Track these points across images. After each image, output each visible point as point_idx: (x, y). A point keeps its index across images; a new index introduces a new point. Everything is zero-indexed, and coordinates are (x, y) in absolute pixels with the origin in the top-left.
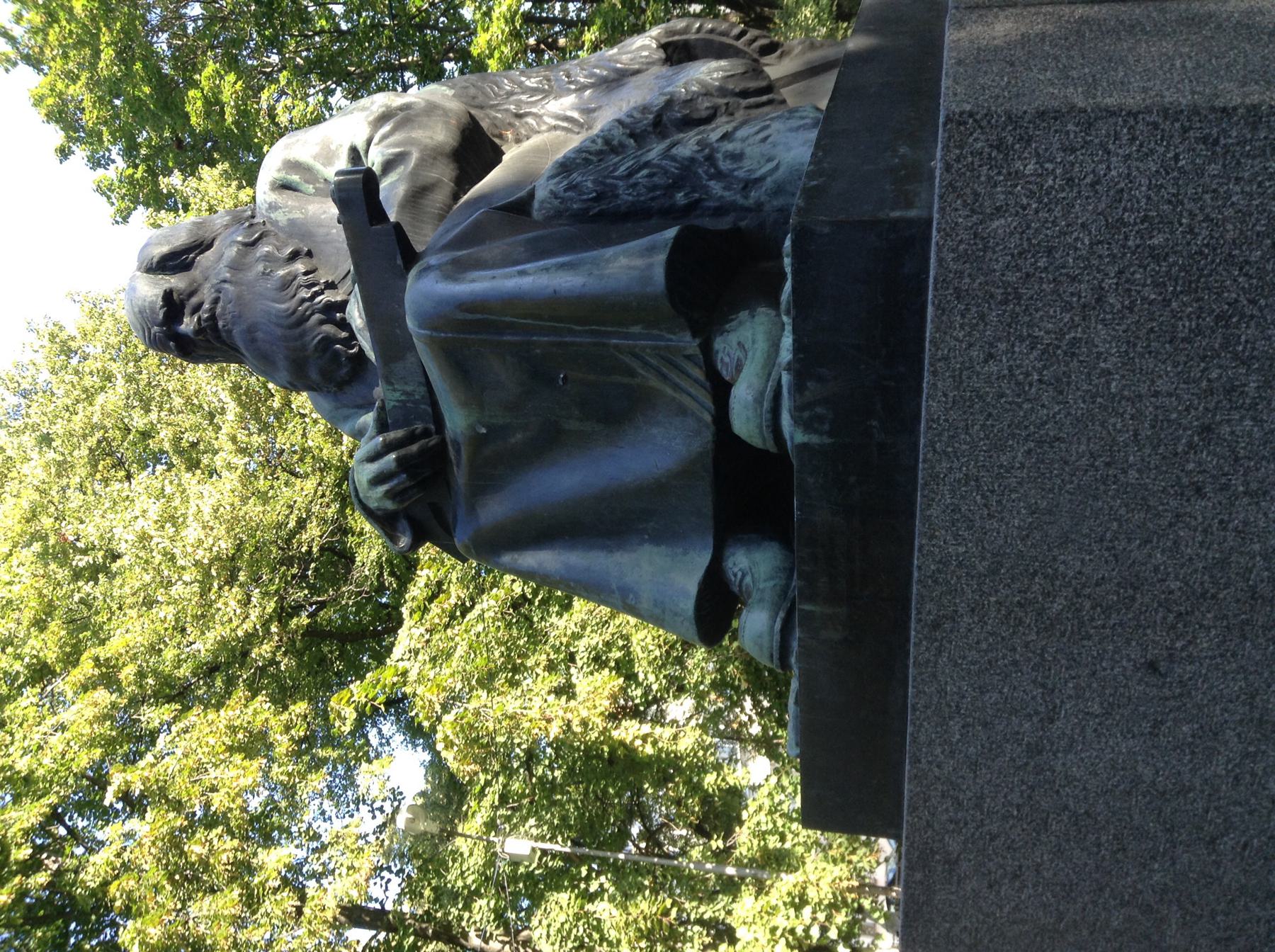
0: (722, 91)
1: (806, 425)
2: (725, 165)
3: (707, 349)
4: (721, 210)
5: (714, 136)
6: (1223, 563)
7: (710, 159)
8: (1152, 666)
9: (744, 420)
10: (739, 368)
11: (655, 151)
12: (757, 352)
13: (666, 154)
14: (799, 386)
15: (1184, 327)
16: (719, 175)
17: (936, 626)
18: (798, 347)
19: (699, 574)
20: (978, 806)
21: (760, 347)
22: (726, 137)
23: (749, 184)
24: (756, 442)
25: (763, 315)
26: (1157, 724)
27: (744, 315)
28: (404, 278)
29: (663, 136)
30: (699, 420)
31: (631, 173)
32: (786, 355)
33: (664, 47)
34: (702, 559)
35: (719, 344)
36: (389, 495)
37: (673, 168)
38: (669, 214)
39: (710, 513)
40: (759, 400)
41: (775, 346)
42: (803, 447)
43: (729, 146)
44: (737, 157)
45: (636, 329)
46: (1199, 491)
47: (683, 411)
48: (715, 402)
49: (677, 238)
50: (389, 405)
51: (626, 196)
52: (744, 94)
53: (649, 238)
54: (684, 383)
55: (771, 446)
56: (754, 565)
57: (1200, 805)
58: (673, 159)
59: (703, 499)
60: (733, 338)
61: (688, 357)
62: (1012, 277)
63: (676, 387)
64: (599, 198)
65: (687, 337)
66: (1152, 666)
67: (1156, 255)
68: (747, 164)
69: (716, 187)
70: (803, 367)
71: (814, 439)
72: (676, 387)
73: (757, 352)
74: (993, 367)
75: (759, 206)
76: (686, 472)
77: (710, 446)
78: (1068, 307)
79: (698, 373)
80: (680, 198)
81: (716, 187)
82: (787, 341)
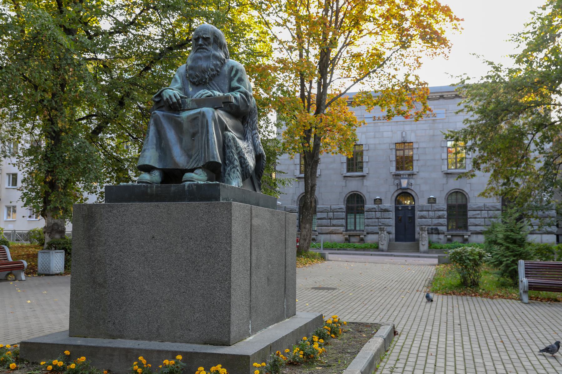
0: (246, 169)
1: (189, 186)
2: (232, 170)
3: (200, 168)
4: (225, 170)
5: (238, 168)
6: (171, 244)
7: (234, 167)
9: (188, 175)
10: (196, 174)
11: (236, 157)
12: (199, 177)
13: (235, 159)
14: (195, 185)
15: (205, 233)
17: (158, 206)
18: (201, 184)
19: (153, 165)
21: (200, 178)
22: (238, 170)
23: (229, 174)
24: (184, 177)
25: (206, 178)
26: (143, 239)
28: (212, 107)
29: (239, 158)
32: (199, 182)
33: (260, 154)
34: (157, 166)
35: (201, 170)
36: (167, 99)
37: (233, 160)
38: (224, 159)
40: (192, 178)
41: (201, 181)
42: (184, 185)
43: (236, 171)
44: (234, 172)
47: (188, 163)
48: (190, 169)
49: (219, 163)
50: (186, 100)
51: (228, 151)
52: (246, 173)
53: (215, 352)
54: (194, 163)
55: (183, 180)
56: (156, 176)
59: (170, 166)
60: (202, 173)
63: (192, 162)
64: (228, 146)
66: (153, 237)
69: (229, 168)
70: (198, 185)
71: (186, 187)
72: (192, 162)
73: (199, 177)
75: (225, 177)
76: (175, 163)
79: (195, 166)
80: (227, 162)
82: (202, 183)
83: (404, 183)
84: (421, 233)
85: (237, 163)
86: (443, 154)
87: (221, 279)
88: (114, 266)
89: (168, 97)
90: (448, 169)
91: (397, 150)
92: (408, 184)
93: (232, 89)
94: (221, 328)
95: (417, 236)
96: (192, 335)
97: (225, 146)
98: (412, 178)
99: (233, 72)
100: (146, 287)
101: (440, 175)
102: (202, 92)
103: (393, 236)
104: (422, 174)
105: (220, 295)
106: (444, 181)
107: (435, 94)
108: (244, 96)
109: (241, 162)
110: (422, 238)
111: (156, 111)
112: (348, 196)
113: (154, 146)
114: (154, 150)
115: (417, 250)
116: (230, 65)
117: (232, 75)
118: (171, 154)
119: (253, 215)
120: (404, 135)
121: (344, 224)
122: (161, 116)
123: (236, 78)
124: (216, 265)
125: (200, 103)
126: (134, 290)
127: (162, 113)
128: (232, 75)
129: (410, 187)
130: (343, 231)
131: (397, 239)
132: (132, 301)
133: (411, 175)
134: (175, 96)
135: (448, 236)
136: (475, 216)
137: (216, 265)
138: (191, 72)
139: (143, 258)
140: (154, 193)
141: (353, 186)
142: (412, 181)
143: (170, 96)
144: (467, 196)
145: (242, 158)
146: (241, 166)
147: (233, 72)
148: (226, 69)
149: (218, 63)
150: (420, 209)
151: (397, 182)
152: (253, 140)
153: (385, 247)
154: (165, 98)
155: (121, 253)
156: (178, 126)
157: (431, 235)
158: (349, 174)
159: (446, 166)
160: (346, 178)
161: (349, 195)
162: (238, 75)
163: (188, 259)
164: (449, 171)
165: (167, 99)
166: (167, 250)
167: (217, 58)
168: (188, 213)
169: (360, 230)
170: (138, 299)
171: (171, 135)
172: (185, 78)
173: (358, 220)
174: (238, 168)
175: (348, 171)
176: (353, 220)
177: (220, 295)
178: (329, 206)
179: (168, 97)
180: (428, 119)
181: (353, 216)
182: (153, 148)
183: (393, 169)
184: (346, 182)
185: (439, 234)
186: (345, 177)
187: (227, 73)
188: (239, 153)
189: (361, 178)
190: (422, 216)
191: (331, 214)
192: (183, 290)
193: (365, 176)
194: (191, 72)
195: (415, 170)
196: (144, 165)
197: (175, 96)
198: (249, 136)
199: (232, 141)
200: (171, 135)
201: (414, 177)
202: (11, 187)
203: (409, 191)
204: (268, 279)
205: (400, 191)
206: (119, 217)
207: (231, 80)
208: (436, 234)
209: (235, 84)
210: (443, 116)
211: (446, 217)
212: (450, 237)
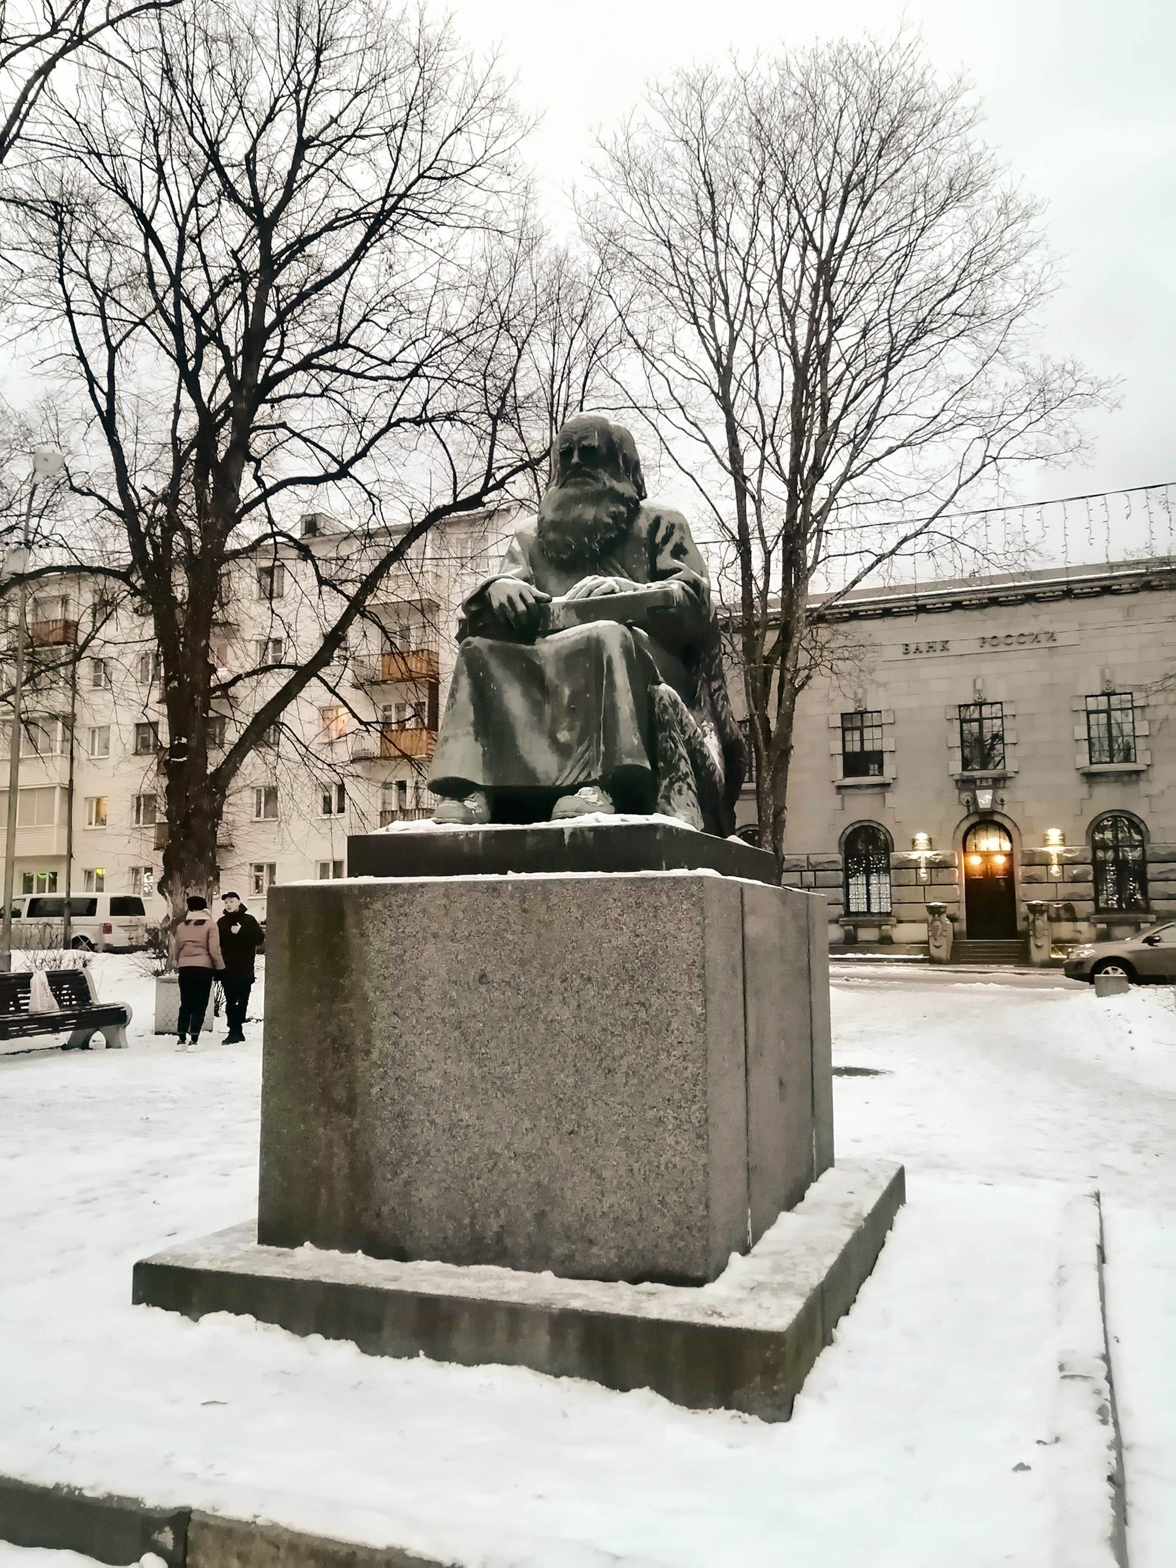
2: (676, 786)
7: (679, 779)
8: (483, 976)
11: (682, 750)
13: (681, 757)
16: (671, 784)
20: (401, 915)
22: (689, 785)
25: (702, 825)
27: (611, 800)
30: (557, 779)
31: (673, 739)
34: (480, 782)
39: (506, 784)
43: (685, 787)
44: (680, 792)
45: (602, 748)
46: (564, 981)
47: (561, 770)
57: (415, 1006)
58: (679, 760)
61: (589, 774)
62: (646, 904)
65: (600, 774)
66: (483, 976)
67: (654, 953)
68: (677, 797)
69: (665, 782)
71: (566, 837)
74: (611, 901)
76: (531, 773)
77: (542, 784)
78: (635, 925)
79: (581, 778)
81: (665, 782)
83: (985, 799)
84: (1031, 917)
85: (684, 767)
86: (1077, 728)
87: (677, 1096)
88: (375, 1055)
89: (505, 600)
90: (1091, 763)
91: (963, 721)
92: (994, 800)
93: (658, 575)
94: (682, 1239)
95: (1021, 925)
96: (598, 1256)
97: (652, 722)
98: (1004, 787)
99: (661, 533)
100: (465, 1115)
101: (1074, 778)
102: (589, 581)
103: (962, 926)
104: (1021, 780)
105: (677, 1143)
106: (1084, 790)
107: (1054, 588)
108: (691, 591)
109: (694, 765)
110: (1034, 930)
111: (470, 639)
112: (848, 832)
113: (471, 729)
114: (471, 739)
115: (1022, 958)
116: (653, 516)
117: (658, 539)
118: (515, 746)
119: (746, 908)
120: (979, 686)
121: (842, 900)
122: (485, 651)
123: (669, 547)
124: (663, 1056)
125: (586, 611)
126: (432, 1122)
127: (489, 641)
128: (658, 539)
129: (999, 808)
130: (841, 916)
131: (970, 933)
132: (428, 1154)
133: (999, 782)
134: (521, 596)
135: (1100, 926)
136: (1162, 876)
137: (663, 1056)
138: (551, 536)
139: (456, 1034)
140: (480, 853)
141: (862, 808)
142: (1002, 794)
143: (510, 599)
144: (1142, 827)
145: (697, 754)
146: (698, 777)
147: (661, 533)
148: (643, 524)
149: (622, 509)
150: (1026, 862)
151: (966, 796)
152: (714, 705)
153: (943, 953)
154: (495, 604)
155: (394, 1020)
156: (533, 677)
157: (1056, 925)
158: (850, 781)
159: (1087, 756)
160: (844, 791)
161: (851, 829)
162: (675, 539)
163: (581, 1038)
164: (1096, 768)
165: (502, 605)
166: (523, 1011)
167: (619, 498)
168: (579, 907)
169: (880, 913)
170: (444, 1149)
171: (514, 700)
172: (536, 551)
173: (873, 889)
174: (689, 780)
175: (848, 773)
176: (863, 889)
177: (677, 1143)
178: (804, 858)
179: (505, 600)
180: (1035, 645)
181: (862, 879)
182: (468, 733)
183: (956, 767)
184: (843, 799)
185: (1074, 919)
186: (839, 788)
187: (644, 535)
188: (688, 743)
189: (877, 790)
190: (1031, 877)
191: (809, 877)
192: (567, 1127)
193: (889, 785)
194: (551, 536)
195: (1011, 766)
196: (446, 780)
197: (521, 596)
198: (704, 698)
199: (671, 710)
200: (514, 700)
201: (1008, 783)
202: (93, 827)
203: (997, 818)
204: (781, 1083)
205: (974, 819)
206: (390, 923)
207: (655, 551)
208: (1068, 920)
209: (665, 561)
210: (1072, 639)
211: (1090, 878)
212: (1104, 926)
